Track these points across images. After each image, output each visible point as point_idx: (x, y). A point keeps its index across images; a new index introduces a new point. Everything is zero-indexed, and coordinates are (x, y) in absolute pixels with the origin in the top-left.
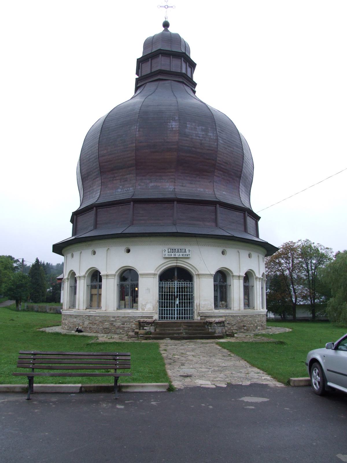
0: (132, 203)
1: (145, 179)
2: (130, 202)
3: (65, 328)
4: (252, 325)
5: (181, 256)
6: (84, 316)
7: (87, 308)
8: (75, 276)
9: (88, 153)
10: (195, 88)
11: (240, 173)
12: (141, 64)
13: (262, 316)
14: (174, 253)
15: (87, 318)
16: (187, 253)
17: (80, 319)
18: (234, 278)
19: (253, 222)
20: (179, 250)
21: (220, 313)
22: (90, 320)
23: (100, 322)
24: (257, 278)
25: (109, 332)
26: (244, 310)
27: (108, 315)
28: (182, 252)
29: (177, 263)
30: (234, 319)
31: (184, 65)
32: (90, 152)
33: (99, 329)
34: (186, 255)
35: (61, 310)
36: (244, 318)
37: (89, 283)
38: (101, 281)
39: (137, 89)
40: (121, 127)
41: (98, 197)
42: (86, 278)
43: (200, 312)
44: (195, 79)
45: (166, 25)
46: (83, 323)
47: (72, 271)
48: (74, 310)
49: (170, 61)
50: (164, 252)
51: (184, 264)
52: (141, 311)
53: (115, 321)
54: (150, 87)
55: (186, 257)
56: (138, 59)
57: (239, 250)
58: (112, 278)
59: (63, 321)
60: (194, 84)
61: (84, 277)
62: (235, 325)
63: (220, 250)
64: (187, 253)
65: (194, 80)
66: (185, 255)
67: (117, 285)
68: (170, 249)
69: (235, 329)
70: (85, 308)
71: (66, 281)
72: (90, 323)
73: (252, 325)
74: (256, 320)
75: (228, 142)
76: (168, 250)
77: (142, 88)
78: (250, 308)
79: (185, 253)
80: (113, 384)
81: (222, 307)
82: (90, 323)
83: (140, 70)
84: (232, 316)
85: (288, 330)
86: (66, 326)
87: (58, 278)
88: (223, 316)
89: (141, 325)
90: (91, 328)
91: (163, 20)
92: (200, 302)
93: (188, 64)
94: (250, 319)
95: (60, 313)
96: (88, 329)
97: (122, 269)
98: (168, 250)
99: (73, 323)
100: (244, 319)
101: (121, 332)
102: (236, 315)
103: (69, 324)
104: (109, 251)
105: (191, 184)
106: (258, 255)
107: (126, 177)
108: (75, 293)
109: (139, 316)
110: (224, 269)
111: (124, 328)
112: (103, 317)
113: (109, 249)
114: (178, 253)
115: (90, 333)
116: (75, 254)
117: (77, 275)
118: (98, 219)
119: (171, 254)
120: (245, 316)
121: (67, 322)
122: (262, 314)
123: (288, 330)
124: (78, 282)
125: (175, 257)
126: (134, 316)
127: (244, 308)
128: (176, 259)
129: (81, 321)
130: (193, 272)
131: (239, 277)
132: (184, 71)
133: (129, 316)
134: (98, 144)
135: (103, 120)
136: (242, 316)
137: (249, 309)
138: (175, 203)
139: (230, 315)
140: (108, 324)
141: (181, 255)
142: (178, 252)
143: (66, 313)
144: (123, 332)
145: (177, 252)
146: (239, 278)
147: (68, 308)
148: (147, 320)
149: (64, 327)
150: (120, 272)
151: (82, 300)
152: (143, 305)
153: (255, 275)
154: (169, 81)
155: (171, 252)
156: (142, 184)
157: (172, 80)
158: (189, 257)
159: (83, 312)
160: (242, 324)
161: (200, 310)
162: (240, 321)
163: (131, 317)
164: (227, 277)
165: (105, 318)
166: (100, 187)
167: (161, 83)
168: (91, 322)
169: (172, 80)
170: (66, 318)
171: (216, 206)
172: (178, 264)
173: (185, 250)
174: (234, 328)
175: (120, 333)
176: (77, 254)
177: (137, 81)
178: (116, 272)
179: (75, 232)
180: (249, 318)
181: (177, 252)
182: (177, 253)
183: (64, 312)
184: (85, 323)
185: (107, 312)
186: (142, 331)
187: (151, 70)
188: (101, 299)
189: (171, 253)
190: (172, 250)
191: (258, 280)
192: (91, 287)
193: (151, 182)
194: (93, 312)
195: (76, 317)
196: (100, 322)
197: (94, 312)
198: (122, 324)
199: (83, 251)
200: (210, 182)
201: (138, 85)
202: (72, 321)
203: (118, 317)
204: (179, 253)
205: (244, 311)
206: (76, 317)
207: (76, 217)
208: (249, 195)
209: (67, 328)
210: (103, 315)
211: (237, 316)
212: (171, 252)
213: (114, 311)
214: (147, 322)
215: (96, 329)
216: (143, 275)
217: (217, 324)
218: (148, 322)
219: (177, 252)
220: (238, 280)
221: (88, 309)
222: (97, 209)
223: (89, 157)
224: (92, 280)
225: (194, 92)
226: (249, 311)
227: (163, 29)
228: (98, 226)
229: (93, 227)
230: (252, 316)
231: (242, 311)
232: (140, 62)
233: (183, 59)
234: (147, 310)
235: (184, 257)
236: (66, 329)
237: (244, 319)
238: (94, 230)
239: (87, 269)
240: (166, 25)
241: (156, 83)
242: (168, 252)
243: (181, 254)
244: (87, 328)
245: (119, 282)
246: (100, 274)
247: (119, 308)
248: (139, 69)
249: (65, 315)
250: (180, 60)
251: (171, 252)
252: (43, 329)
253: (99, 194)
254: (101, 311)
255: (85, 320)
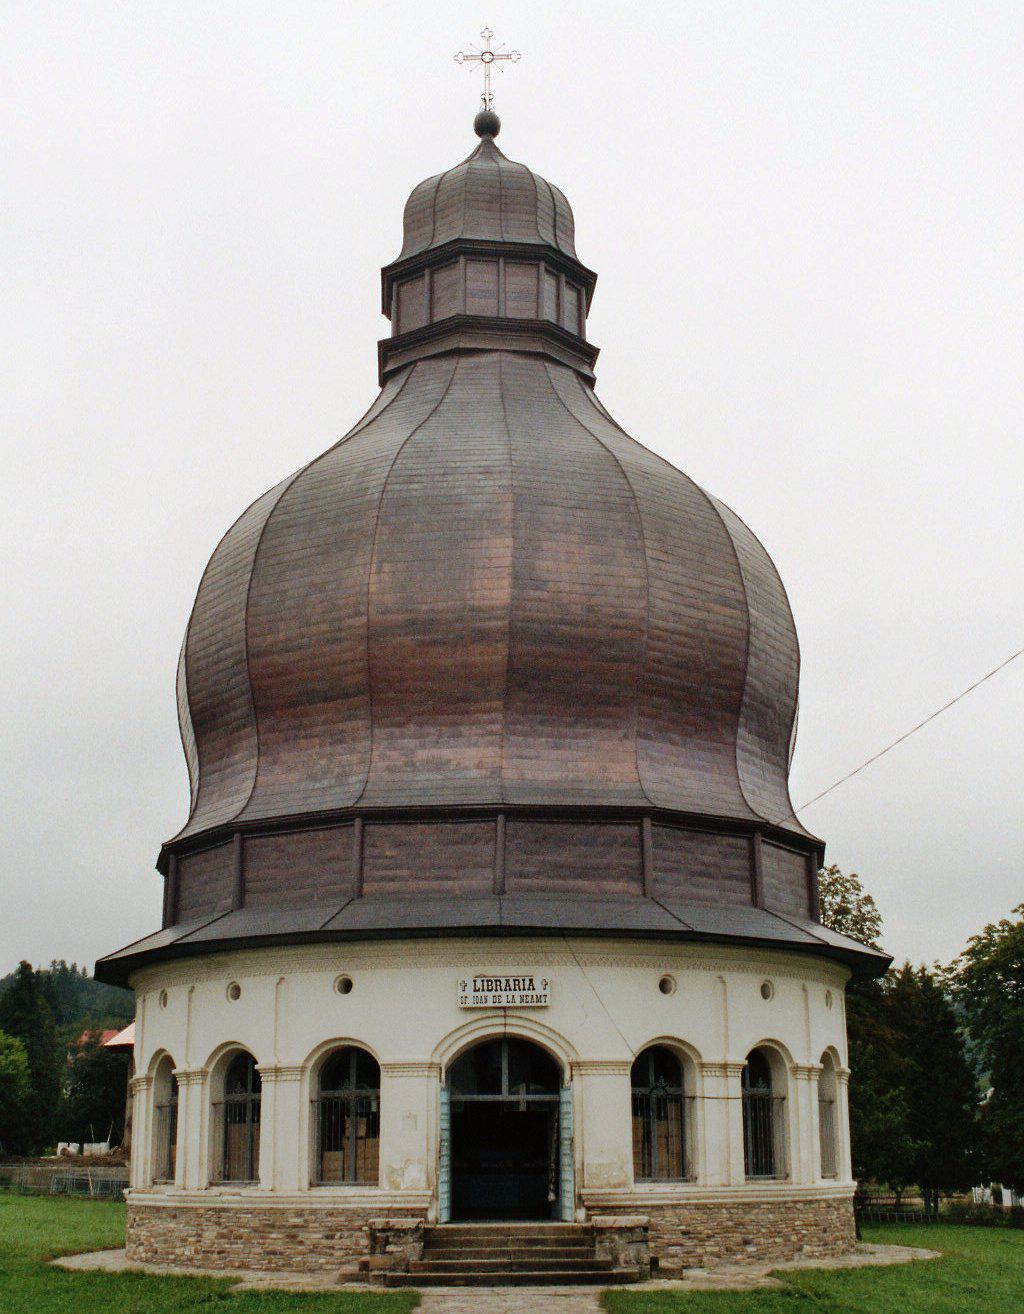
0: (358, 822)
1: (403, 737)
2: (353, 820)
3: (135, 1257)
4: (777, 1240)
5: (518, 1004)
6: (202, 1211)
7: (211, 1184)
8: (174, 1072)
9: (213, 640)
10: (592, 365)
11: (735, 693)
12: (399, 286)
13: (823, 1205)
14: (494, 993)
15: (213, 1219)
16: (539, 991)
17: (187, 1223)
18: (705, 1073)
19: (795, 863)
20: (511, 983)
21: (653, 1196)
22: (219, 1224)
23: (256, 1230)
24: (796, 1069)
25: (283, 1265)
26: (747, 1184)
27: (281, 1206)
28: (522, 987)
29: (505, 1025)
30: (705, 1216)
31: (548, 284)
32: (220, 635)
33: (251, 1256)
34: (535, 997)
35: (126, 1191)
36: (746, 1213)
37: (221, 1096)
38: (257, 1088)
39: (384, 379)
40: (318, 554)
41: (247, 794)
42: (209, 1076)
43: (583, 1191)
44: (591, 338)
45: (487, 126)
46: (200, 1236)
47: (163, 1055)
48: (169, 1190)
49: (499, 272)
50: (460, 988)
51: (531, 1029)
52: (386, 1192)
53: (303, 1227)
54: (430, 378)
55: (535, 1004)
56: (384, 271)
57: (722, 973)
58: (294, 1078)
59: (132, 1231)
60: (591, 354)
61: (203, 1073)
62: (709, 1237)
63: (653, 977)
64: (539, 991)
65: (589, 340)
66: (529, 999)
67: (312, 1102)
68: (483, 981)
69: (712, 1254)
70: (205, 1182)
71: (141, 1088)
72: (222, 1236)
73: (777, 1240)
74: (793, 1219)
75: (691, 593)
76: (475, 981)
77: (401, 379)
78: (774, 1178)
79: (530, 993)
80: (85, 1146)
81: (668, 1176)
82: (222, 1236)
83: (394, 304)
84: (698, 1207)
85: (925, 1254)
86: (141, 1249)
87: (108, 1044)
88: (667, 1206)
89: (380, 1238)
90: (223, 1252)
91: (475, 110)
92: (583, 1158)
93: (563, 279)
94: (771, 1216)
95: (121, 1199)
96: (215, 1256)
97: (317, 1056)
98: (475, 981)
99: (164, 1234)
100: (748, 1217)
101: (322, 1264)
102: (714, 1205)
103: (153, 1240)
104: (283, 986)
105: (556, 747)
106: (804, 986)
107: (341, 726)
108: (173, 1140)
109: (381, 1209)
110: (669, 1042)
111: (332, 1251)
112: (266, 1211)
113: (282, 979)
114: (508, 993)
115: (224, 1268)
116: (172, 992)
117: (180, 1068)
118: (249, 875)
119: (486, 997)
120: (749, 1207)
121: (143, 1233)
122: (825, 1200)
123: (925, 1254)
124: (182, 1090)
125: (497, 1005)
126: (364, 1209)
127: (747, 1179)
128: (501, 1013)
129: (192, 1230)
130: (564, 1057)
131: (724, 1067)
132: (548, 314)
133: (348, 1210)
134: (244, 612)
135: (257, 523)
136: (738, 1205)
137: (772, 1181)
138: (501, 818)
139: (690, 1204)
140: (280, 1236)
141: (518, 999)
142: (508, 988)
143: (139, 1200)
144: (327, 1263)
145: (506, 990)
146: (726, 1072)
147: (149, 1183)
148: (397, 1222)
149: (135, 1253)
150: (317, 1061)
151: (194, 1155)
152: (393, 1171)
153: (791, 1060)
154: (495, 357)
155: (483, 990)
156: (394, 754)
157: (506, 351)
158: (543, 1004)
159: (272, 1199)
160: (738, 1235)
161: (584, 1187)
162: (730, 1223)
163: (355, 1213)
164: (686, 1069)
165: (271, 1220)
166: (256, 759)
167: (465, 362)
168: (225, 1231)
169: (506, 351)
170: (141, 1219)
171: (641, 826)
172: (509, 1030)
173: (531, 981)
174: (709, 1249)
175: (321, 1268)
176: (178, 994)
177: (386, 349)
178: (307, 1060)
179: (173, 914)
180: (763, 1213)
181: (503, 988)
182: (504, 994)
183: (133, 1197)
184: (206, 1235)
185: (188, 1193)
186: (378, 1259)
187: (431, 314)
188: (258, 1154)
189: (486, 993)
190: (488, 981)
191: (803, 1075)
192: (226, 1108)
193: (423, 746)
194: (231, 1196)
195: (174, 1214)
196: (256, 1231)
197: (235, 1198)
198: (327, 1237)
199: (199, 987)
200: (626, 736)
201: (389, 367)
202: (160, 1231)
203: (313, 1212)
204: (510, 993)
205: (747, 1188)
206: (175, 1217)
207: (175, 858)
208: (782, 762)
209: (143, 1255)
210: (262, 1206)
211: (720, 1206)
212: (486, 988)
213: (299, 1194)
214: (396, 1227)
215: (242, 1256)
216: (392, 1067)
217: (621, 1235)
218: (398, 1230)
219: (503, 988)
220: (721, 1080)
221: (217, 1185)
222: (243, 841)
223: (218, 651)
224: (229, 1087)
225: (590, 382)
226: (765, 1189)
227: (478, 140)
228: (248, 898)
229: (230, 900)
230: (775, 1206)
231: (736, 1188)
232: (394, 278)
233: (542, 265)
234: (407, 1189)
235: (528, 1005)
236: (141, 1259)
237: (748, 1217)
238: (234, 913)
239: (213, 1049)
240: (487, 126)
241: (446, 365)
242: (475, 991)
243: (517, 994)
244: (213, 1252)
245: (318, 1093)
246: (256, 1067)
247: (320, 1177)
248: (391, 299)
249: (139, 1209)
250: (534, 271)
251: (486, 988)
252: (62, 1262)
253: (250, 784)
254: (258, 1194)
255: (205, 1224)
